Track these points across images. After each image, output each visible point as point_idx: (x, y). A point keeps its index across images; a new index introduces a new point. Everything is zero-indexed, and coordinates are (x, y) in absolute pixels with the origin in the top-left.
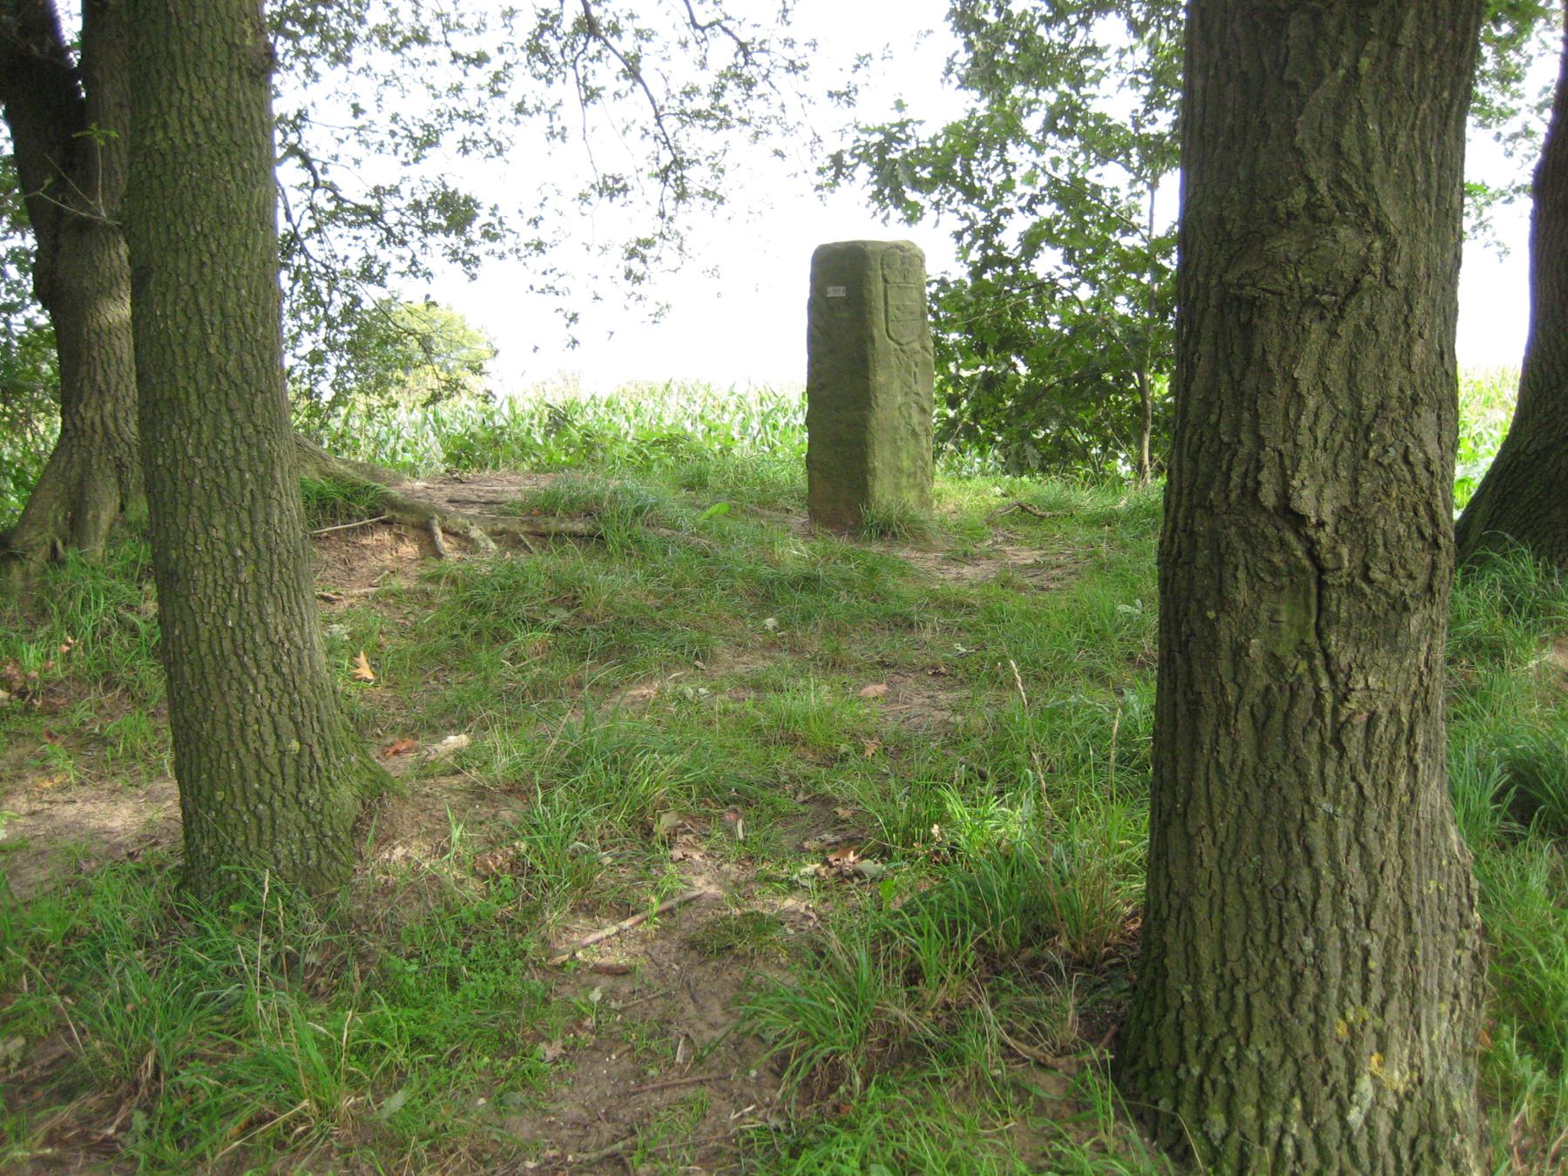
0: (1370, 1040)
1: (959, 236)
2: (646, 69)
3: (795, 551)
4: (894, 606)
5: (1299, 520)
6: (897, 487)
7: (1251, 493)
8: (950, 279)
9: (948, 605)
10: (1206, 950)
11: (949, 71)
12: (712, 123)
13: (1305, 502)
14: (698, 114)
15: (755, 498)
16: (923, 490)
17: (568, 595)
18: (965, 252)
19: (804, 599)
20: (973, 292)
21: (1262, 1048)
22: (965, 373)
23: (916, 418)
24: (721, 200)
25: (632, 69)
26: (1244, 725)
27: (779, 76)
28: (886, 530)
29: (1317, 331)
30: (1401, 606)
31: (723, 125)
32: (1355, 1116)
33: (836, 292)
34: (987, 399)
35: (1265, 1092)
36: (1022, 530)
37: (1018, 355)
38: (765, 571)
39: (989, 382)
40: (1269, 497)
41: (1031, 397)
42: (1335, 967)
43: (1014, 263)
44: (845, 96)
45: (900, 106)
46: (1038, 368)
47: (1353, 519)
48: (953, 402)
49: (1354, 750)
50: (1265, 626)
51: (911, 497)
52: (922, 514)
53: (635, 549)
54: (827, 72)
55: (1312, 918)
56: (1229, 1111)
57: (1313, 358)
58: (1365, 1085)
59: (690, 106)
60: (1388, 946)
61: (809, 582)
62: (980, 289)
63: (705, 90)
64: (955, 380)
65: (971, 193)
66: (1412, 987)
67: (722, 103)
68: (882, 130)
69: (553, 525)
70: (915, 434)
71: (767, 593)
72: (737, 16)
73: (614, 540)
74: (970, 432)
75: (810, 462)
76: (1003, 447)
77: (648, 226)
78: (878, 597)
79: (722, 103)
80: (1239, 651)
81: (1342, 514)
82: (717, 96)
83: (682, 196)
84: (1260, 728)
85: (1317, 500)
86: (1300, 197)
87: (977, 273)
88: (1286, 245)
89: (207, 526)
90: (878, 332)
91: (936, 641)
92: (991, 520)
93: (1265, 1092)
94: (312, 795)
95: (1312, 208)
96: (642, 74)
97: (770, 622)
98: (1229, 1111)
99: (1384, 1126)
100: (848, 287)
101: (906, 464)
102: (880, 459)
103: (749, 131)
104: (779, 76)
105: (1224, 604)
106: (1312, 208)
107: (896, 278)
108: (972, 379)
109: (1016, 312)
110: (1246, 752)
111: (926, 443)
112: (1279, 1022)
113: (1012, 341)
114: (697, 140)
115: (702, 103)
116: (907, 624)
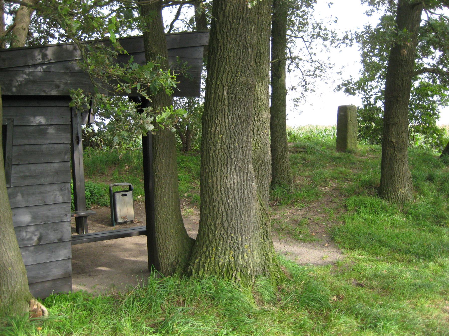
0: (400, 188)
1: (362, 98)
2: (300, 66)
3: (337, 154)
4: (352, 161)
5: (392, 142)
6: (351, 145)
7: (388, 140)
8: (360, 108)
9: (360, 161)
10: (385, 180)
11: (360, 72)
12: (313, 77)
13: (393, 140)
14: (310, 75)
15: (329, 148)
16: (355, 146)
17: (304, 159)
18: (364, 102)
19: (338, 161)
20: (364, 110)
21: (390, 188)
22: (362, 126)
23: (355, 134)
24: (314, 91)
25: (297, 66)
26: (388, 159)
27: (328, 69)
28: (349, 152)
29: (394, 127)
30: (401, 149)
31: (315, 77)
32: (398, 195)
33: (342, 114)
34: (366, 131)
35: (391, 193)
36: (372, 153)
37: (373, 122)
38: (333, 156)
39: (367, 128)
40: (390, 140)
41: (375, 130)
42: (396, 181)
43: (372, 105)
44: (340, 73)
45: (351, 76)
46: (377, 125)
47: (397, 142)
48: (360, 131)
49: (398, 162)
50: (390, 151)
51: (353, 147)
52: (355, 150)
53: (312, 153)
54: (337, 69)
55: (394, 176)
56: (388, 195)
57: (393, 129)
58: (399, 192)
59: (308, 73)
60: (401, 180)
61: (339, 158)
62: (366, 110)
63: (312, 71)
64: (360, 127)
65: (365, 91)
66: (404, 183)
67: (315, 73)
68: (347, 81)
69: (298, 150)
70: (354, 137)
71: (333, 159)
72: (320, 60)
73: (309, 151)
74: (363, 137)
75: (337, 141)
76: (369, 140)
77: (299, 95)
78: (350, 160)
79: (315, 73)
80: (388, 153)
81: (396, 141)
82: (314, 72)
83: (306, 90)
84: (390, 160)
85: (394, 140)
86: (392, 116)
87: (365, 106)
88: (391, 120)
89: (280, 144)
90: (349, 120)
91: (358, 164)
92: (367, 152)
93: (391, 193)
94: (289, 175)
95: (393, 117)
96: (299, 67)
97: (334, 163)
98: (388, 195)
99: (401, 196)
100: (344, 113)
101: (353, 141)
102: (349, 140)
103: (320, 78)
104: (328, 69)
105: (386, 149)
106: (393, 117)
107: (352, 112)
108: (364, 127)
109: (373, 114)
110: (389, 162)
111: (356, 138)
112: (392, 186)
113: (371, 119)
114: (309, 80)
115: (311, 73)
116: (355, 164)
